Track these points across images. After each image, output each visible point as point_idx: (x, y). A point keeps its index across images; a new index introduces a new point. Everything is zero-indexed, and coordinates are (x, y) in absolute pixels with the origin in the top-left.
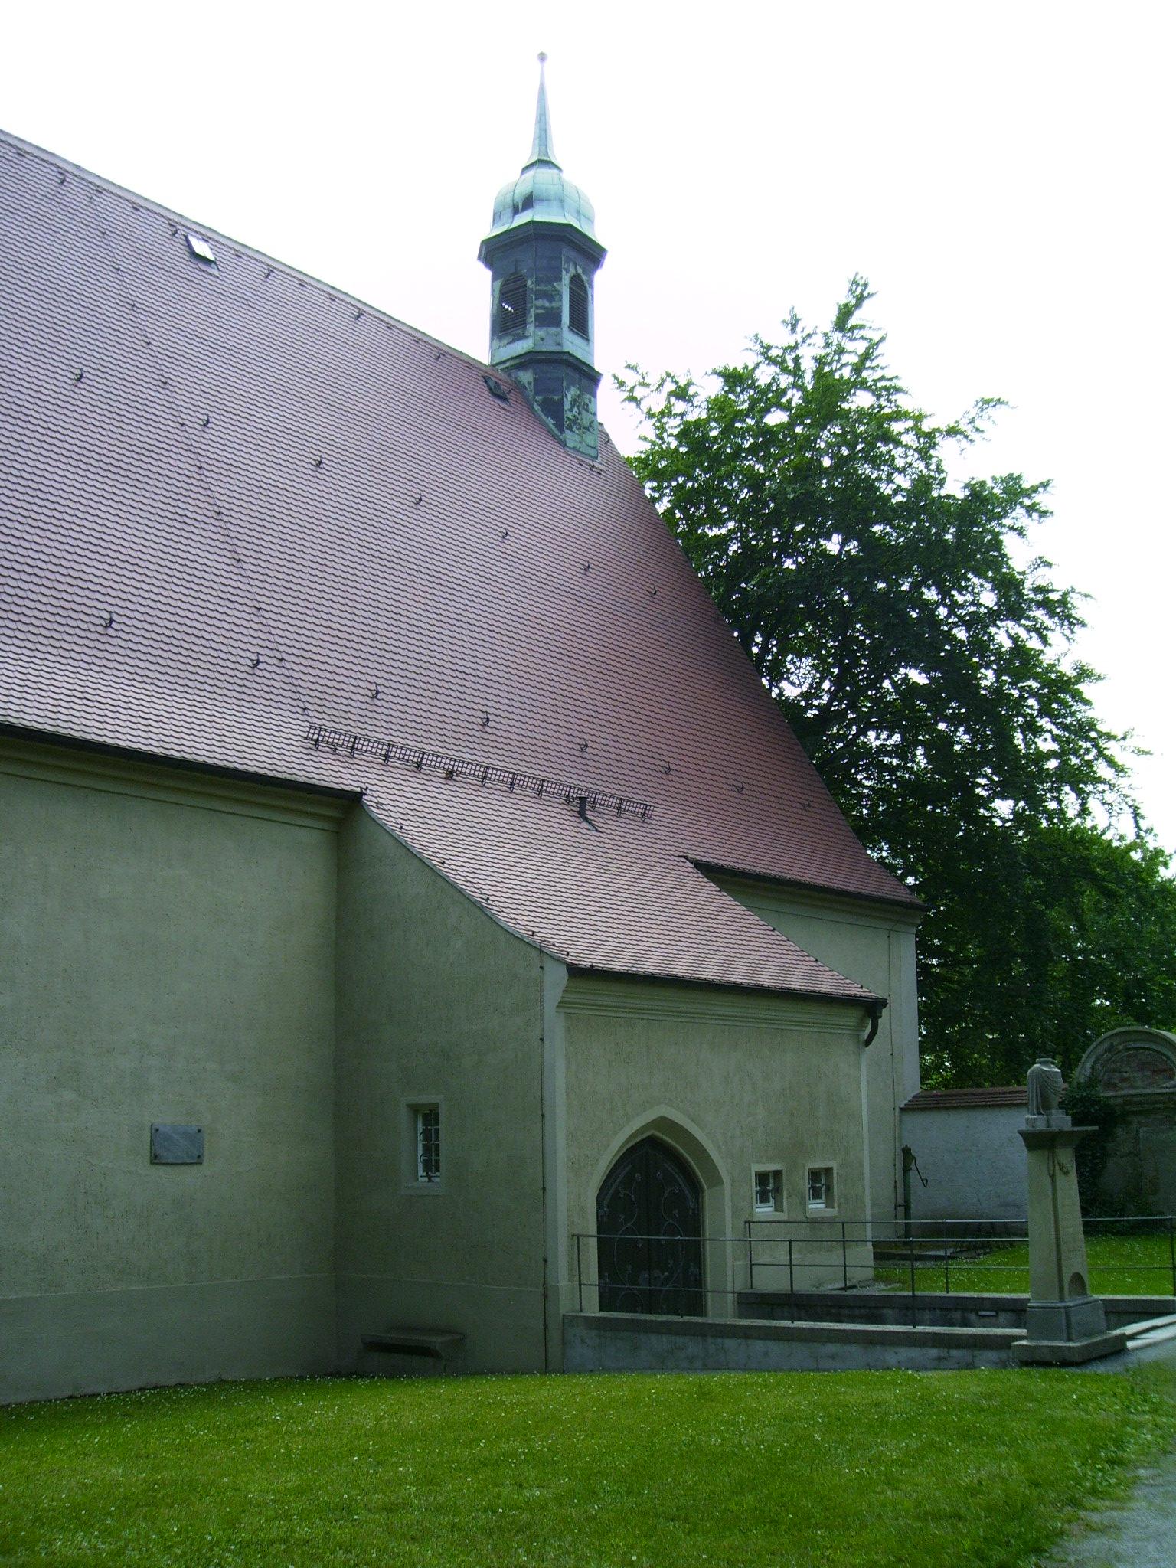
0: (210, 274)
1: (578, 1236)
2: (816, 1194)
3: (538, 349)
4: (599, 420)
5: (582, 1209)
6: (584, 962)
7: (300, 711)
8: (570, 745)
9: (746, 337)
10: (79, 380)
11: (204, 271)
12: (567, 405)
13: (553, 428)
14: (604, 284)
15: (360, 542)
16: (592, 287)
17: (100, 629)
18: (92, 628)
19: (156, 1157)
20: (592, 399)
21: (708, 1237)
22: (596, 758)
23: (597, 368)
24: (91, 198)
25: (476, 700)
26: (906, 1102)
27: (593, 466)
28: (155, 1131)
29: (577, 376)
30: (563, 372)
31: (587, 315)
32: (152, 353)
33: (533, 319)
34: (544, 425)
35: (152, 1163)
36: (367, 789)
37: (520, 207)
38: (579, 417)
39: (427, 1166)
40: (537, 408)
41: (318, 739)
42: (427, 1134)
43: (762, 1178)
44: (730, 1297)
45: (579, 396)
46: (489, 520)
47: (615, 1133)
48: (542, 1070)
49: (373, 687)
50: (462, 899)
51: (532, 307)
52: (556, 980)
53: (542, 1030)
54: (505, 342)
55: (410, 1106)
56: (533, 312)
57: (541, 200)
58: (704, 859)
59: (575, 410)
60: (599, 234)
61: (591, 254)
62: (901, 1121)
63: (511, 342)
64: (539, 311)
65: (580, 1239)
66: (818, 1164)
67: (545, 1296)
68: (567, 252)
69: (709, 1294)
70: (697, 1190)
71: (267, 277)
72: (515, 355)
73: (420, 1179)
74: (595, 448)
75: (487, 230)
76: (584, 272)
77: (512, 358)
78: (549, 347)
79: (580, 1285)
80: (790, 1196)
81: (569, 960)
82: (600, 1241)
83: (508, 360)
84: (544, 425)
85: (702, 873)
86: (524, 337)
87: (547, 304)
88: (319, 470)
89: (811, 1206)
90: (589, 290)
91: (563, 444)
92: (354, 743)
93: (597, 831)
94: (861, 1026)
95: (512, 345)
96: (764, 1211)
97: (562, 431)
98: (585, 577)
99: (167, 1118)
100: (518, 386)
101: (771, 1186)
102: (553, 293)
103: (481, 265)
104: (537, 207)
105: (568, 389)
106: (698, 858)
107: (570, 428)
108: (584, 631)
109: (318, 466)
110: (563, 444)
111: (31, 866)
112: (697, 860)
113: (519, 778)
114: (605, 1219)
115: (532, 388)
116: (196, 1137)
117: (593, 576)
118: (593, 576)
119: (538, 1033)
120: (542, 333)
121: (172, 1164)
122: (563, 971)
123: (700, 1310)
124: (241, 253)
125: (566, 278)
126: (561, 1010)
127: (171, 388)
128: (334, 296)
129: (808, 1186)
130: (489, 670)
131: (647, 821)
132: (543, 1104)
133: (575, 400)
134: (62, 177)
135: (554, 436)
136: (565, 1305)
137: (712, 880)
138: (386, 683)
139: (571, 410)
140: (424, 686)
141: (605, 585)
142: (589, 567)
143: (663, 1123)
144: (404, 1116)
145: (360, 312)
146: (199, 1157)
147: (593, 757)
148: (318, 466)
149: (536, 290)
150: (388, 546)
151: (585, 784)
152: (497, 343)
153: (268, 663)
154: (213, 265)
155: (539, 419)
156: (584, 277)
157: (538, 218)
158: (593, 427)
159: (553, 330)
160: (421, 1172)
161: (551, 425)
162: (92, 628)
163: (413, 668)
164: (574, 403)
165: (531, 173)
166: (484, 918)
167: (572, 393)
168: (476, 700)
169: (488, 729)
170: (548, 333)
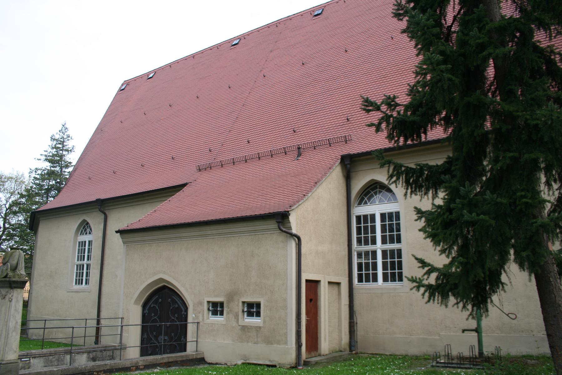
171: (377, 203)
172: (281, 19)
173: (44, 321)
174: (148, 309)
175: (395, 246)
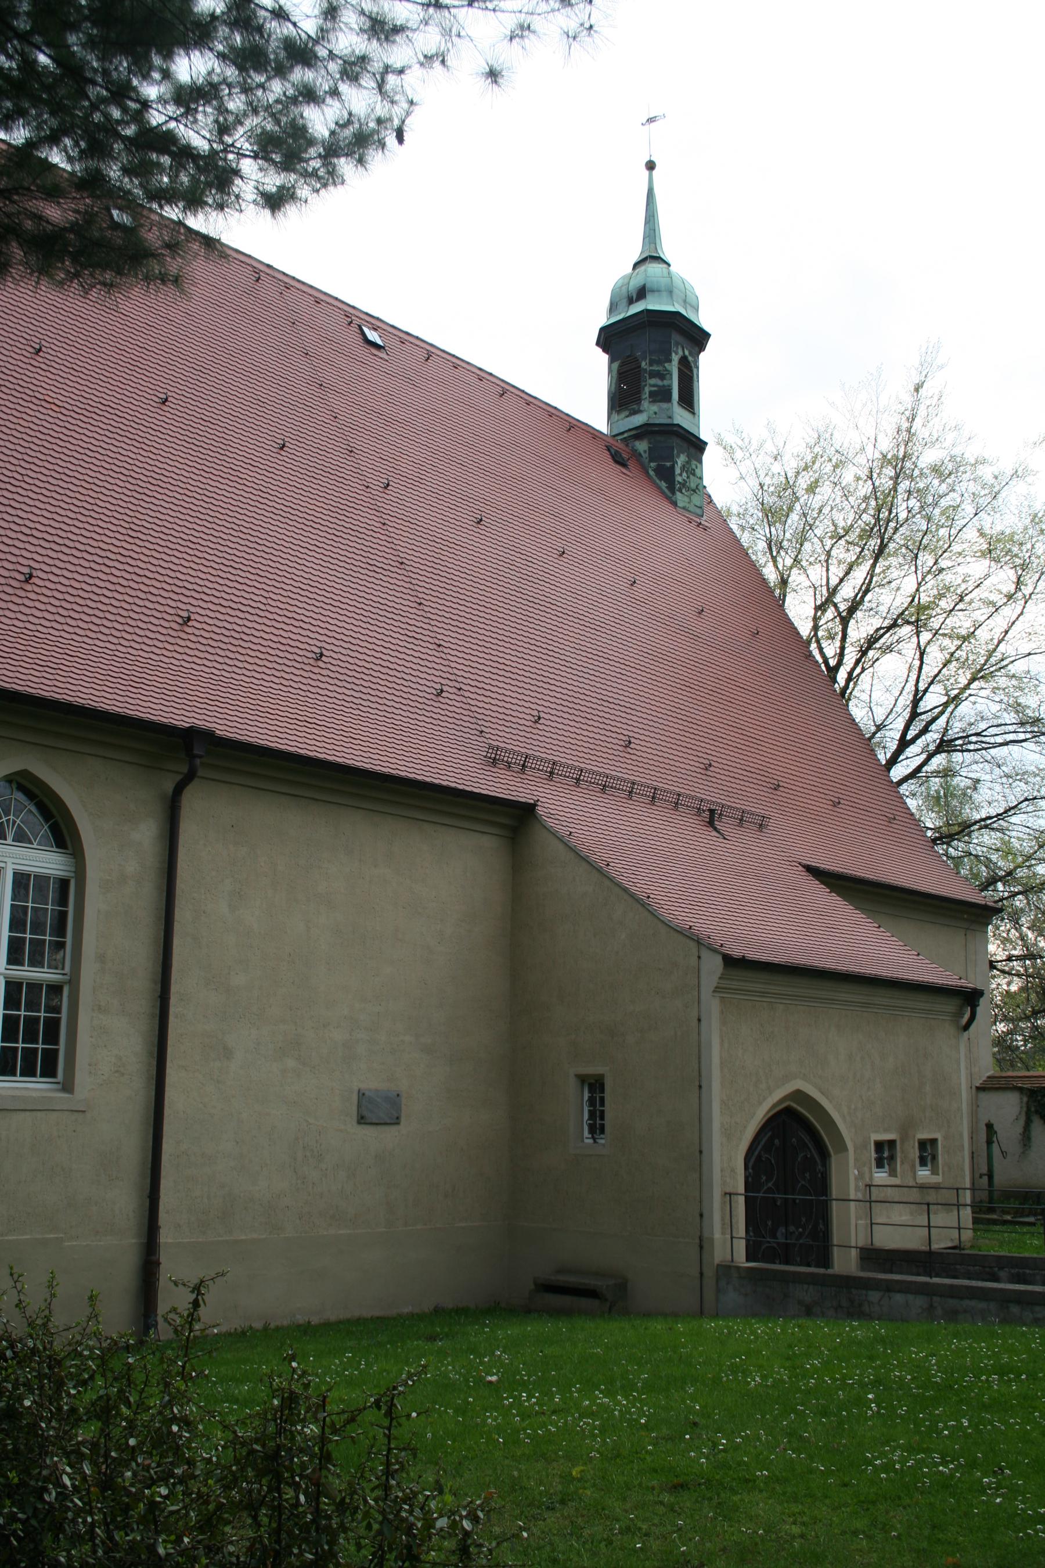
1: (730, 1194)
2: (923, 1162)
3: (651, 421)
4: (705, 484)
5: (733, 1170)
6: (737, 951)
7: (478, 733)
8: (697, 764)
9: (882, 364)
10: (282, 449)
11: (375, 355)
12: (678, 471)
13: (666, 491)
14: (707, 362)
15: (517, 589)
16: (698, 368)
17: (312, 661)
18: (306, 661)
21: (834, 1197)
22: (718, 776)
24: (281, 293)
25: (619, 725)
26: (981, 1082)
27: (700, 523)
28: (361, 1094)
30: (675, 441)
31: (693, 389)
32: (339, 426)
33: (647, 395)
34: (659, 488)
35: (359, 1123)
36: (538, 800)
39: (592, 1130)
40: (652, 473)
41: (495, 758)
42: (592, 1101)
43: (879, 1146)
44: (854, 1253)
45: (687, 462)
46: (619, 570)
47: (760, 1103)
48: (699, 1046)
49: (535, 713)
50: (626, 897)
51: (646, 385)
52: (713, 965)
53: (699, 1011)
54: (623, 415)
55: (577, 1076)
56: (647, 390)
57: (652, 291)
58: (814, 864)
59: (684, 474)
60: (704, 320)
61: (698, 338)
62: (977, 1096)
63: (627, 417)
65: (960, 1191)
67: (701, 1247)
68: (676, 337)
69: (835, 1248)
70: (824, 1155)
71: (427, 360)
72: (631, 427)
74: (701, 508)
75: (602, 319)
76: (690, 354)
77: (630, 430)
79: (732, 1238)
80: (902, 1163)
81: (724, 950)
82: (746, 1197)
84: (659, 488)
85: (813, 876)
87: (660, 383)
88: (480, 526)
89: (920, 1173)
90: (695, 370)
91: (675, 504)
92: (525, 761)
93: (725, 839)
95: (628, 419)
96: (881, 1176)
97: (673, 493)
98: (699, 619)
99: (373, 1084)
100: (636, 455)
101: (886, 1155)
103: (599, 350)
104: (649, 297)
105: (678, 456)
106: (809, 863)
107: (680, 491)
108: (701, 666)
109: (478, 523)
110: (675, 504)
112: (808, 865)
113: (659, 792)
114: (750, 1179)
115: (647, 455)
116: (394, 1101)
117: (706, 618)
118: (706, 618)
120: (654, 408)
121: (377, 1124)
122: (719, 960)
123: (825, 1261)
124: (405, 338)
125: (675, 358)
126: (715, 994)
127: (356, 456)
128: (482, 376)
129: (918, 1154)
130: (627, 699)
131: (764, 830)
132: (700, 1076)
133: (684, 466)
134: (257, 276)
136: (719, 1254)
137: (822, 883)
138: (546, 710)
139: (681, 475)
140: (576, 713)
141: (716, 626)
142: (702, 611)
143: (799, 1095)
144: (572, 1083)
145: (505, 390)
146: (398, 1118)
147: (715, 775)
148: (478, 523)
150: (540, 592)
151: (714, 796)
152: (615, 416)
154: (382, 350)
156: (690, 359)
158: (699, 489)
159: (665, 405)
160: (586, 1134)
161: (664, 488)
162: (306, 661)
163: (566, 697)
164: (683, 468)
165: (642, 269)
166: (646, 913)
167: (681, 459)
168: (619, 725)
169: (629, 750)
170: (660, 408)
171: (9, 841)
172: (250, 256)
173: (926, 1206)
174: (855, 1167)
175: (27, 973)
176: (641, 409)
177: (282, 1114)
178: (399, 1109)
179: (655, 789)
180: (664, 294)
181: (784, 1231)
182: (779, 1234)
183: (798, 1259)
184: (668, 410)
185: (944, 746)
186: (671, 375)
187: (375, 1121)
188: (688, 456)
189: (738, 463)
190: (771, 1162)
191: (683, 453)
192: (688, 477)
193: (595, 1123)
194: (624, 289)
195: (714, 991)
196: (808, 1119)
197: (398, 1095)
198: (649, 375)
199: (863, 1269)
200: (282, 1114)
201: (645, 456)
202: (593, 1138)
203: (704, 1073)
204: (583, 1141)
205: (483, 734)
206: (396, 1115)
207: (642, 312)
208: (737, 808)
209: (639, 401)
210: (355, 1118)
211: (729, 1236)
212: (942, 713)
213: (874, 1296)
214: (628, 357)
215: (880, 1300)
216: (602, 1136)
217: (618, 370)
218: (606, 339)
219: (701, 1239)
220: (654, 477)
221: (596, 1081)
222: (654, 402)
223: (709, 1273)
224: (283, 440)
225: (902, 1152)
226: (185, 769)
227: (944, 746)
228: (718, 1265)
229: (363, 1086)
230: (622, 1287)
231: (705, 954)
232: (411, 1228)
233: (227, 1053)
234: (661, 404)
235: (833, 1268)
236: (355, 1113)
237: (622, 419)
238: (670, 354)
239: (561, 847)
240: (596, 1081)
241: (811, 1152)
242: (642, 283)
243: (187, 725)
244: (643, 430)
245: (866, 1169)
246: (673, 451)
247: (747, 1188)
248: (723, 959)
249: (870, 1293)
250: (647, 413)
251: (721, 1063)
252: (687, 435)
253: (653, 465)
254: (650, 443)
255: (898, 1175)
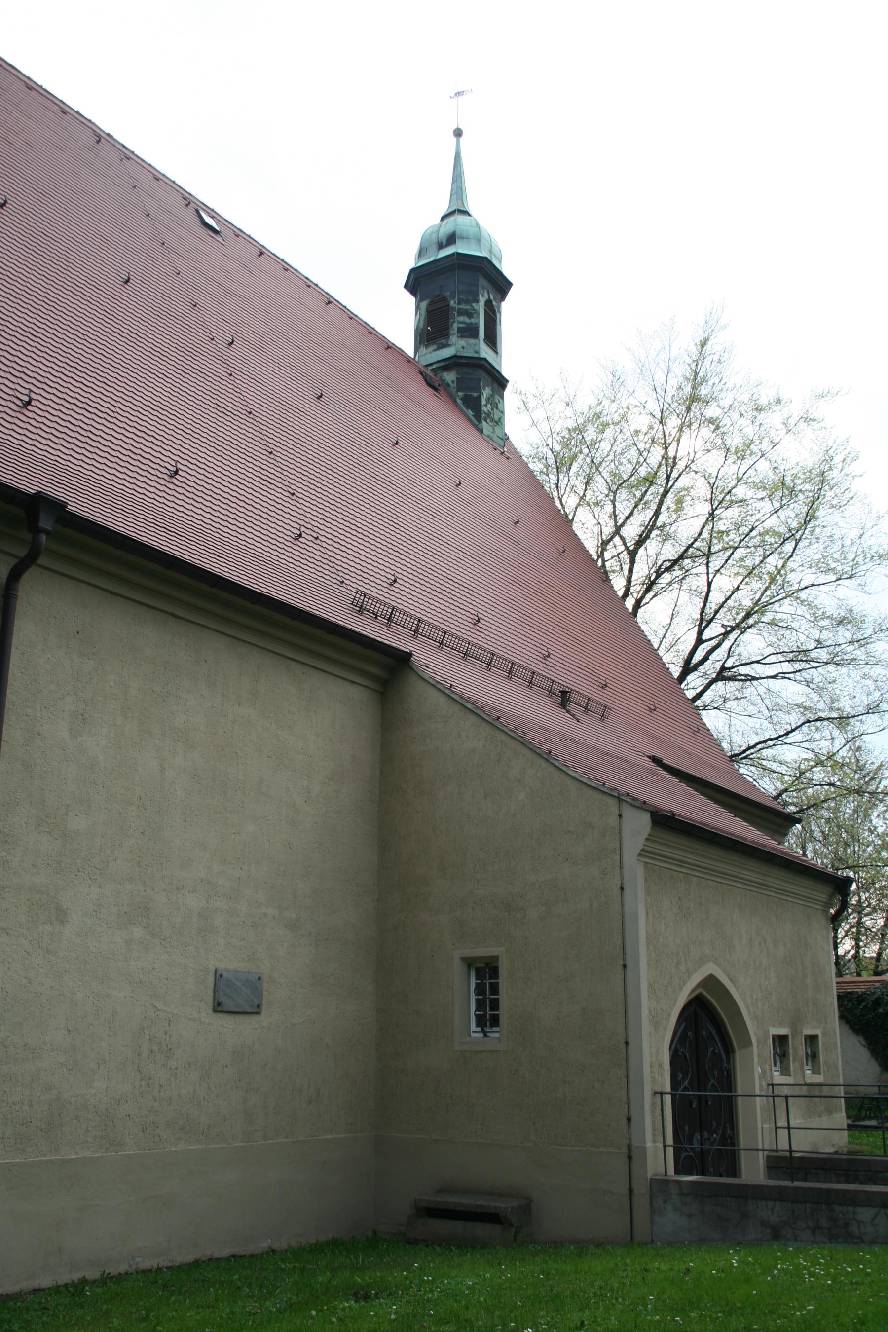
0: (218, 241)
3: (459, 354)
5: (660, 1066)
9: (675, 316)
12: (484, 402)
13: (473, 418)
16: (500, 313)
19: (219, 1004)
20: (501, 400)
23: (504, 373)
28: (218, 976)
29: (490, 379)
30: (482, 375)
31: (496, 331)
33: (456, 331)
34: (466, 416)
35: (215, 1011)
37: (444, 243)
38: (492, 412)
39: (480, 1021)
40: (459, 401)
42: (479, 989)
51: (454, 322)
53: (622, 878)
54: (431, 349)
56: (455, 326)
57: (462, 238)
59: (489, 406)
60: (507, 269)
61: (502, 286)
63: (435, 350)
64: (461, 325)
66: (808, 1031)
67: (630, 1158)
68: (482, 281)
70: (729, 1050)
72: (440, 359)
73: (474, 1035)
75: (409, 262)
77: (439, 362)
78: (470, 353)
83: (435, 363)
86: (447, 345)
87: (467, 320)
90: (498, 315)
91: (481, 431)
93: (578, 721)
94: (829, 905)
95: (437, 352)
97: (480, 421)
99: (230, 963)
102: (472, 312)
105: (484, 389)
110: (481, 431)
111: (112, 684)
115: (455, 385)
116: (255, 984)
119: (618, 882)
120: (463, 342)
121: (235, 1013)
122: (645, 819)
124: (239, 233)
125: (482, 301)
128: (309, 284)
132: (624, 953)
135: (474, 426)
139: (486, 406)
144: (458, 968)
149: (458, 309)
153: (307, 538)
155: (461, 411)
156: (494, 303)
157: (460, 251)
159: (472, 341)
161: (470, 416)
164: (488, 400)
166: (551, 769)
167: (486, 393)
170: (468, 343)
176: (449, 343)
177: (125, 997)
178: (260, 995)
179: (513, 663)
180: (473, 241)
181: (699, 1137)
182: (695, 1141)
183: (712, 1170)
184: (475, 345)
185: (723, 675)
186: (478, 314)
187: (232, 1009)
188: (492, 390)
189: (530, 410)
190: (686, 1056)
191: (488, 386)
192: (492, 409)
193: (485, 1016)
194: (434, 237)
195: (640, 855)
196: (714, 1008)
197: (259, 979)
198: (458, 313)
199: (770, 1177)
200: (125, 997)
201: (453, 385)
202: (483, 1031)
203: (629, 950)
204: (470, 1036)
205: (344, 585)
206: (257, 1003)
207: (453, 254)
208: (585, 695)
209: (447, 335)
210: (211, 1004)
211: (661, 1146)
212: (718, 646)
213: (865, 1214)
214: (438, 296)
215: (873, 1219)
216: (494, 1029)
217: (427, 309)
218: (416, 280)
219: (629, 1147)
220: (462, 406)
221: (487, 964)
222: (462, 337)
223: (641, 1189)
224: (129, 273)
225: (794, 1048)
226: (22, 552)
227: (723, 675)
228: (651, 1179)
229: (221, 966)
230: (527, 1207)
231: (627, 811)
232: (270, 1141)
233: (61, 915)
234: (468, 340)
235: (740, 1177)
236: (210, 999)
237: (430, 353)
238: (478, 296)
239: (442, 699)
240: (487, 964)
241: (718, 1046)
242: (452, 230)
243: (33, 492)
244: (451, 361)
245: (767, 1066)
246: (480, 383)
247: (672, 1089)
248: (651, 816)
249: (859, 1209)
250: (456, 347)
251: (647, 938)
252: (492, 370)
253: (460, 394)
254: (458, 374)
255: (792, 1075)
